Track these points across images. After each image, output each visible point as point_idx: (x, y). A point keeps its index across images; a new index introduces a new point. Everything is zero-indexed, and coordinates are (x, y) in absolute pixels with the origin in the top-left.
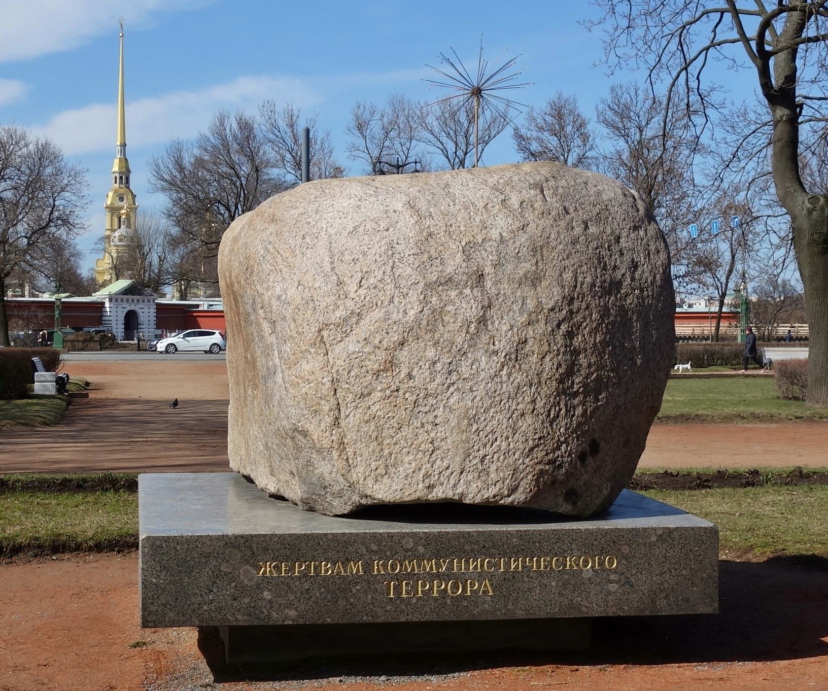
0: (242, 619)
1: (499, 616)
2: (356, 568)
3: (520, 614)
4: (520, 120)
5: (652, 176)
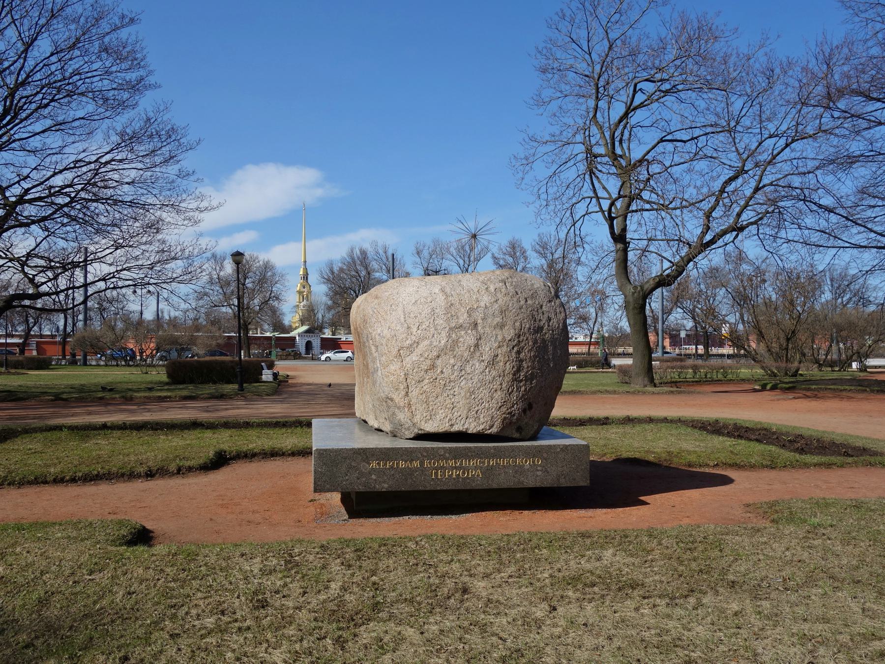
0: (362, 489)
2: (416, 464)
3: (495, 486)
4: (494, 250)
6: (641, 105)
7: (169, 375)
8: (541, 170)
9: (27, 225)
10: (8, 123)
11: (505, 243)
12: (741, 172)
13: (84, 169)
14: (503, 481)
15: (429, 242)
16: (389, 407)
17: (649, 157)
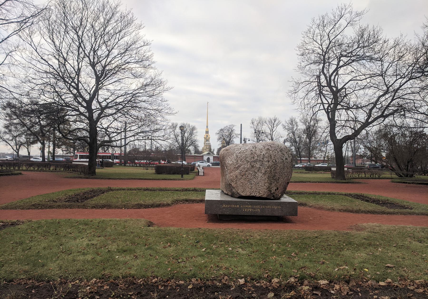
0: (220, 213)
1: (261, 215)
2: (238, 206)
3: (264, 215)
4: (284, 123)
5: (310, 132)
6: (342, 66)
7: (156, 171)
8: (301, 94)
9: (108, 116)
10: (102, 80)
11: (288, 119)
12: (386, 92)
13: (128, 96)
14: (267, 213)
15: (257, 118)
16: (230, 187)
17: (346, 87)
